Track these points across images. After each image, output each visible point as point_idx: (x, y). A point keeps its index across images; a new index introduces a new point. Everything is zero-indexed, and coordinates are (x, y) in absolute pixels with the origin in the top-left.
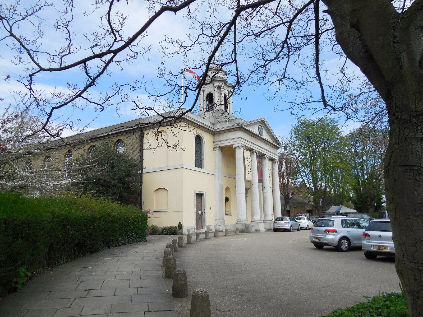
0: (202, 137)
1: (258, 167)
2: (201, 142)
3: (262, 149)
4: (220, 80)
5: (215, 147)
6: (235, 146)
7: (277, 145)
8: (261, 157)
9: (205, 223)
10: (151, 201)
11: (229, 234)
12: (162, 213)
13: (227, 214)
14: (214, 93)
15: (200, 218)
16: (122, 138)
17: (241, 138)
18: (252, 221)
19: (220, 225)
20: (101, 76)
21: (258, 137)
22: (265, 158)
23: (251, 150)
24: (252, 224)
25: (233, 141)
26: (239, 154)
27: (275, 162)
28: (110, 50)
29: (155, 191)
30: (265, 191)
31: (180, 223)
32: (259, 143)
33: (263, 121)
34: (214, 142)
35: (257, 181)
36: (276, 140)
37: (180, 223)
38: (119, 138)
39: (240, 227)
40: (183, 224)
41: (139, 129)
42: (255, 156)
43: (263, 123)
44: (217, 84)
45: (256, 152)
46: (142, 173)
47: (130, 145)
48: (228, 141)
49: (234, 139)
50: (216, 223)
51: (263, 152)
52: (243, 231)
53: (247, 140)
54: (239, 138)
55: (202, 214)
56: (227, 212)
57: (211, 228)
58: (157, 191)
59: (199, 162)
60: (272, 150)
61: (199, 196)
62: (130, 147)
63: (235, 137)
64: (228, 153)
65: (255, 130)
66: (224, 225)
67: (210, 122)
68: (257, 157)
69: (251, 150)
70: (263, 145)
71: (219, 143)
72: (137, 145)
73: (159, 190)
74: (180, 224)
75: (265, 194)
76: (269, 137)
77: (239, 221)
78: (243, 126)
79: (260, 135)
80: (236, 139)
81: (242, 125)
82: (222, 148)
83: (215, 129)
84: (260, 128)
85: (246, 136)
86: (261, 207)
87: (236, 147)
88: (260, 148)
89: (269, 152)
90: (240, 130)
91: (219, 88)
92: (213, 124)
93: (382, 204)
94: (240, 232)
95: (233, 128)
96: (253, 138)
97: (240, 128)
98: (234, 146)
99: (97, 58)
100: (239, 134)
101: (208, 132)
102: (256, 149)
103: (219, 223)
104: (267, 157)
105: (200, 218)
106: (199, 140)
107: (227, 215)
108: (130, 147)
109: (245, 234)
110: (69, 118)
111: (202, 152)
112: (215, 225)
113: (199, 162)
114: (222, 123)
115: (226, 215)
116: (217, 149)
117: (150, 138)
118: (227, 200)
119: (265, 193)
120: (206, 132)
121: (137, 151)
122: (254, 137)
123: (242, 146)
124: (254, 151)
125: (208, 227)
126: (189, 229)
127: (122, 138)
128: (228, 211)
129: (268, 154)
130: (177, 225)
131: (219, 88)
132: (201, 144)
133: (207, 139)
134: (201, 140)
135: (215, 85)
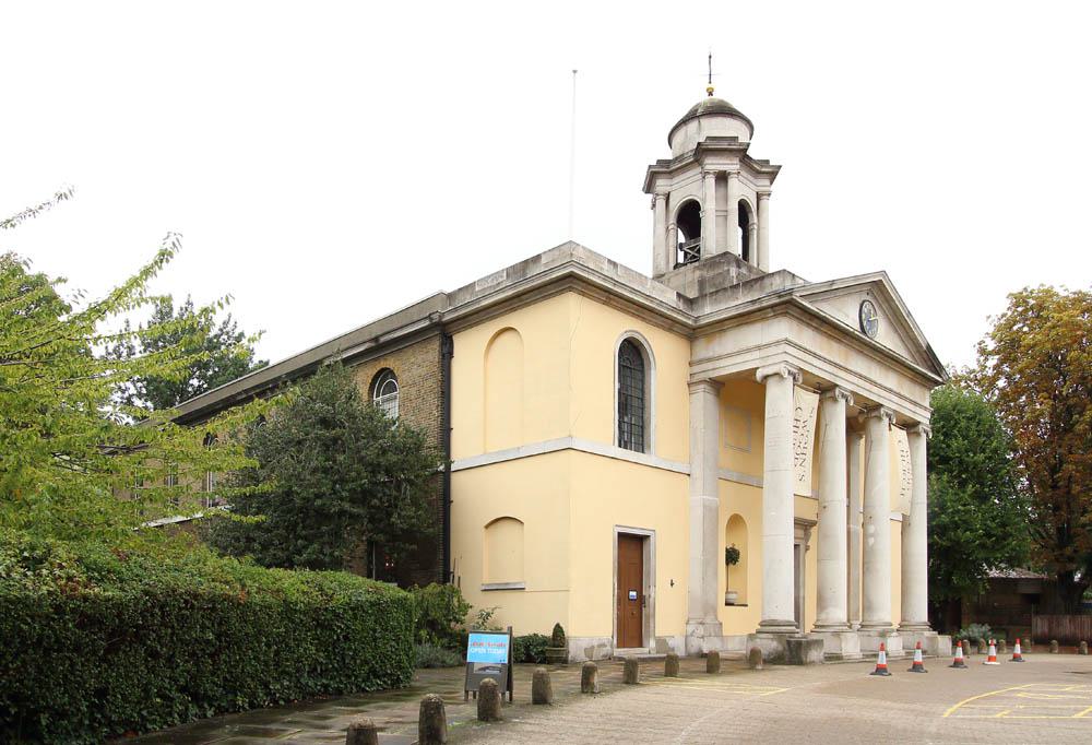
0: (646, 346)
2: (642, 365)
3: (868, 386)
4: (725, 150)
5: (696, 379)
7: (929, 374)
9: (652, 629)
10: (478, 559)
11: (722, 666)
12: (508, 594)
13: (732, 601)
14: (704, 200)
15: (632, 615)
16: (390, 363)
17: (788, 342)
18: (816, 626)
19: (703, 637)
20: (525, 321)
22: (879, 418)
23: (825, 390)
24: (815, 637)
25: (757, 354)
29: (487, 527)
30: (871, 529)
31: (558, 626)
32: (859, 364)
37: (558, 626)
38: (383, 364)
39: (768, 645)
40: (570, 631)
41: (437, 329)
43: (878, 290)
44: (714, 164)
45: (843, 396)
46: (447, 473)
47: (414, 384)
48: (739, 359)
49: (759, 348)
50: (690, 629)
51: (874, 395)
52: (776, 660)
53: (813, 350)
54: (778, 343)
55: (641, 601)
56: (732, 597)
57: (671, 643)
58: (493, 527)
59: (633, 426)
61: (632, 547)
62: (413, 391)
64: (740, 398)
65: (846, 314)
66: (720, 635)
67: (679, 295)
69: (825, 390)
71: (710, 366)
74: (558, 630)
75: (871, 541)
76: (900, 344)
77: (767, 625)
78: (796, 296)
80: (768, 348)
81: (791, 294)
82: (719, 386)
84: (865, 310)
85: (808, 337)
86: (495, 311)
87: (766, 377)
88: (861, 382)
89: (895, 399)
90: (785, 314)
91: (722, 178)
92: (690, 302)
94: (765, 662)
95: (757, 306)
96: (835, 345)
97: (790, 306)
98: (759, 375)
100: (782, 328)
102: (846, 383)
103: (701, 631)
104: (887, 415)
105: (632, 615)
106: (632, 356)
107: (732, 604)
109: (786, 667)
110: (672, 584)
112: (686, 636)
113: (633, 426)
115: (727, 604)
116: (702, 386)
117: (469, 348)
118: (732, 557)
119: (872, 535)
122: (839, 341)
124: (837, 393)
125: (661, 642)
127: (390, 363)
128: (736, 593)
129: (890, 403)
130: (549, 633)
131: (722, 178)
132: (643, 372)
133: (664, 352)
134: (644, 356)
135: (708, 167)
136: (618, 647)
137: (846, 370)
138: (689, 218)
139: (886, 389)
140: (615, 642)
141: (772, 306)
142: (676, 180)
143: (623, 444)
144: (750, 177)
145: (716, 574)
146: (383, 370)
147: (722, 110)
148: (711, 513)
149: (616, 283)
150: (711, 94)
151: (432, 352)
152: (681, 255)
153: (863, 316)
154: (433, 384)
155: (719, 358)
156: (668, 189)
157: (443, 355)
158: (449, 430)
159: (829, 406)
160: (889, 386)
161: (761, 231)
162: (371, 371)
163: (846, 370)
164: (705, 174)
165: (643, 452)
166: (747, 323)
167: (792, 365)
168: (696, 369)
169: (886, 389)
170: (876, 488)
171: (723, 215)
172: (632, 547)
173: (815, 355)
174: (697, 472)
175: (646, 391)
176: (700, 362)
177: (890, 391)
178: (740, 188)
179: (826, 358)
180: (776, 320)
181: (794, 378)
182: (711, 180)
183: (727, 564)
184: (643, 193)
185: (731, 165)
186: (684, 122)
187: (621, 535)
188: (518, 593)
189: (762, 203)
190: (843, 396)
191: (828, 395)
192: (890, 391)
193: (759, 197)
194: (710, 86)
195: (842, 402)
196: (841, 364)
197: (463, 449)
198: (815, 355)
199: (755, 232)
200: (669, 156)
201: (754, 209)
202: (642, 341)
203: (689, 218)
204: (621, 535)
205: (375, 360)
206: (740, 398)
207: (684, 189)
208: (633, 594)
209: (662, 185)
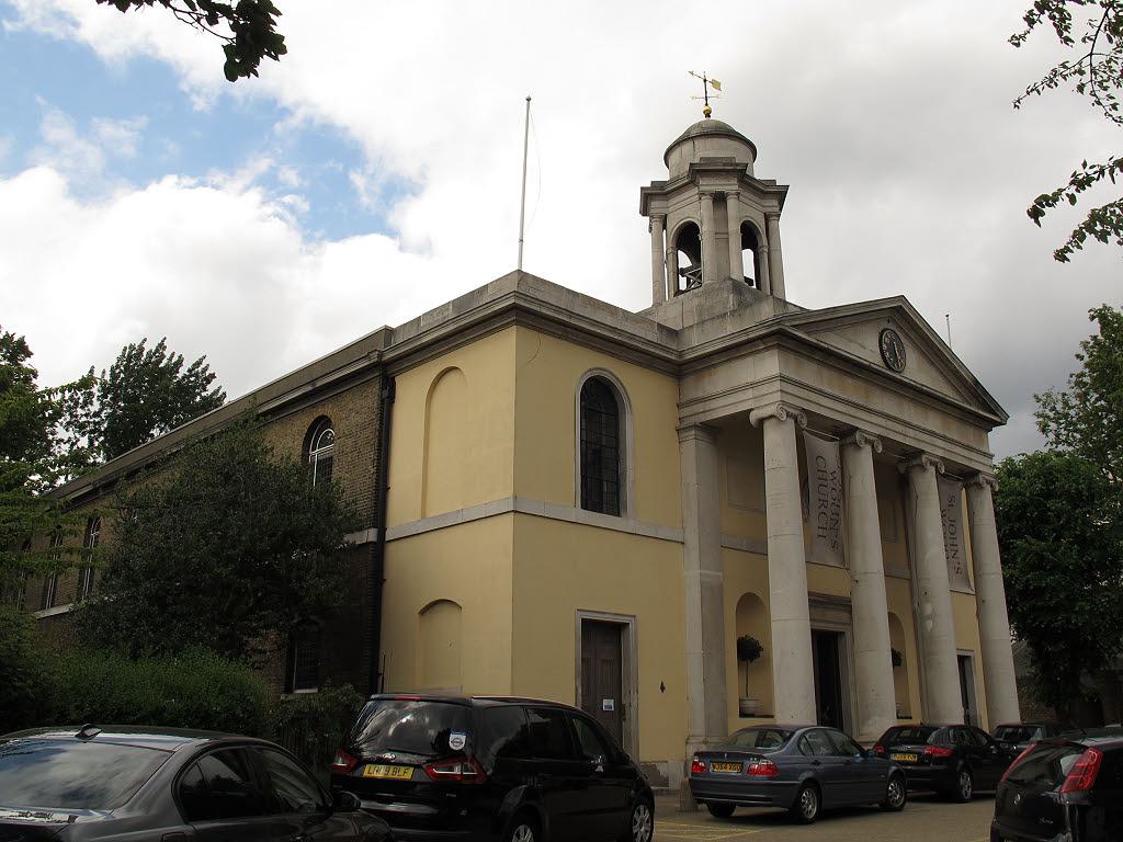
0: (618, 386)
3: (899, 428)
5: (688, 422)
6: (760, 416)
7: (981, 412)
13: (750, 711)
16: (327, 410)
21: (885, 379)
22: (923, 468)
25: (750, 393)
26: (779, 448)
27: (980, 486)
29: (423, 612)
36: (975, 391)
38: (320, 411)
45: (867, 441)
46: (380, 545)
48: (731, 399)
51: (910, 439)
56: (750, 705)
60: (955, 431)
62: (350, 442)
63: (759, 377)
65: (865, 347)
69: (844, 435)
70: (910, 413)
72: (367, 433)
73: (437, 608)
76: (935, 374)
79: (890, 368)
83: (681, 354)
87: (761, 421)
88: (890, 424)
89: (940, 443)
93: (162, 365)
96: (849, 381)
98: (753, 417)
99: (225, 60)
101: (650, 366)
102: (868, 425)
108: (350, 442)
110: (663, 688)
111: (621, 446)
113: (601, 483)
114: (708, 325)
117: (411, 389)
119: (929, 617)
120: (640, 364)
123: (788, 415)
127: (327, 410)
131: (719, 199)
137: (870, 411)
138: (688, 238)
139: (924, 431)
142: (673, 201)
144: (754, 198)
147: (724, 133)
149: (571, 314)
150: (708, 115)
151: (369, 399)
152: (683, 282)
153: (885, 346)
154: (370, 434)
156: (664, 211)
157: (382, 401)
159: (850, 453)
161: (773, 253)
162: (306, 420)
163: (870, 411)
165: (619, 515)
166: (737, 358)
167: (790, 405)
168: (686, 411)
169: (924, 431)
170: (927, 557)
171: (722, 237)
174: (692, 539)
175: (621, 438)
177: (932, 434)
179: (835, 398)
181: (796, 421)
182: (707, 202)
184: (70, 205)
185: (730, 186)
186: (678, 143)
187: (584, 621)
189: (772, 224)
190: (867, 441)
191: (849, 440)
192: (932, 434)
193: (767, 217)
194: (707, 108)
195: (868, 448)
196: (861, 403)
197: (403, 510)
199: (766, 255)
200: (666, 178)
201: (762, 229)
202: (613, 380)
203: (688, 238)
204: (584, 621)
205: (313, 406)
206: (736, 441)
207: (692, 208)
208: (608, 703)
209: (655, 205)
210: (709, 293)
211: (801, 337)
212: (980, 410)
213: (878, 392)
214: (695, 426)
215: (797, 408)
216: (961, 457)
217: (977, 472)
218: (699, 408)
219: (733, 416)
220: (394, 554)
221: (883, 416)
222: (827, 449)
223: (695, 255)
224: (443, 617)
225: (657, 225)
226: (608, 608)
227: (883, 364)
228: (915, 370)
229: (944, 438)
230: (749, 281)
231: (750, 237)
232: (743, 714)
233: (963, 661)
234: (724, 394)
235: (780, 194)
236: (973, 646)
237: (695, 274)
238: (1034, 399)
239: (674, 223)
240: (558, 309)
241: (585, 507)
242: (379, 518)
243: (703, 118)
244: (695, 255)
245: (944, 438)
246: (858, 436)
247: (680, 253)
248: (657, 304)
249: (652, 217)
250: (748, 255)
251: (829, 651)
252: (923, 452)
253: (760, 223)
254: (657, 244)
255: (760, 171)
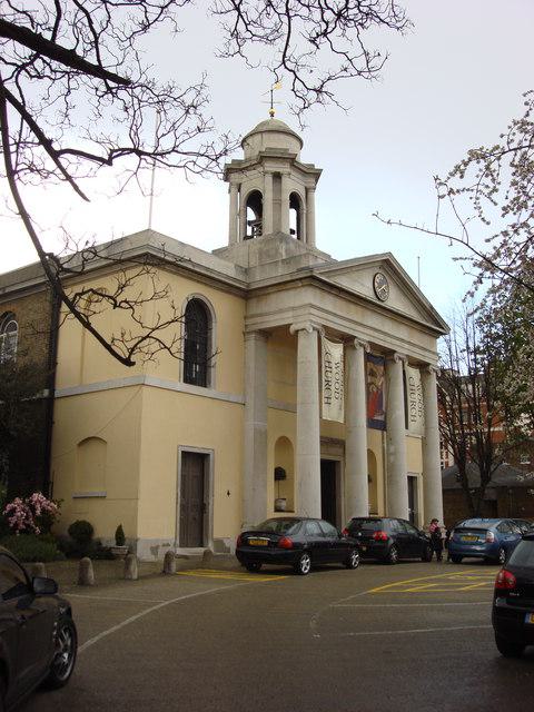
1: (368, 385)
3: (382, 336)
8: (381, 358)
17: (312, 306)
21: (375, 306)
23: (347, 341)
25: (290, 314)
26: (307, 348)
28: (9, 107)
29: (81, 444)
32: (374, 320)
33: (387, 261)
34: (245, 318)
35: (365, 424)
36: (430, 313)
42: (434, 382)
43: (387, 267)
44: (271, 167)
46: (51, 400)
48: (276, 317)
56: (283, 504)
59: (197, 365)
60: (418, 338)
65: (363, 287)
68: (368, 357)
69: (347, 341)
70: (388, 326)
82: (267, 335)
85: (329, 303)
87: (297, 331)
88: (376, 334)
89: (407, 346)
91: (277, 177)
98: (292, 329)
100: (309, 296)
102: (363, 336)
106: (197, 315)
118: (280, 475)
119: (392, 454)
120: (222, 290)
121: (43, 342)
123: (314, 329)
125: (219, 543)
126: (157, 547)
129: (402, 350)
131: (277, 177)
133: (222, 309)
136: (180, 546)
139: (398, 339)
140: (178, 542)
141: (301, 279)
143: (188, 379)
145: (265, 486)
146: (7, 313)
148: (262, 436)
152: (249, 230)
155: (267, 314)
158: (55, 364)
160: (401, 337)
164: (265, 173)
168: (249, 321)
169: (398, 339)
171: (278, 203)
172: (407, 428)
173: (335, 315)
176: (253, 316)
178: (292, 184)
180: (303, 289)
182: (269, 178)
183: (276, 479)
185: (284, 168)
186: (251, 135)
187: (186, 455)
188: (101, 501)
192: (402, 340)
193: (307, 190)
198: (335, 315)
203: (255, 200)
206: (281, 340)
207: (254, 181)
210: (268, 240)
211: (323, 279)
212: (432, 325)
213: (369, 313)
214: (255, 331)
215: (318, 324)
216: (418, 355)
217: (428, 364)
218: (258, 320)
219: (280, 327)
220: (61, 409)
221: (373, 329)
222: (336, 351)
223: (259, 211)
224: (94, 447)
225: (234, 190)
226: (197, 445)
227: (374, 297)
228: (395, 301)
229: (409, 343)
230: (292, 232)
231: (295, 201)
232: (277, 510)
233: (412, 480)
234: (275, 313)
235: (317, 175)
236: (417, 470)
237: (258, 225)
238: (433, 183)
239: (246, 190)
240: (207, 269)
241: (186, 381)
242: (50, 382)
243: (268, 117)
244: (259, 211)
245: (409, 343)
246: (396, 355)
247: (249, 209)
248: (231, 244)
249: (231, 184)
250: (293, 213)
251: (330, 471)
252: (395, 351)
253: (302, 193)
254: (233, 203)
255: (304, 158)
